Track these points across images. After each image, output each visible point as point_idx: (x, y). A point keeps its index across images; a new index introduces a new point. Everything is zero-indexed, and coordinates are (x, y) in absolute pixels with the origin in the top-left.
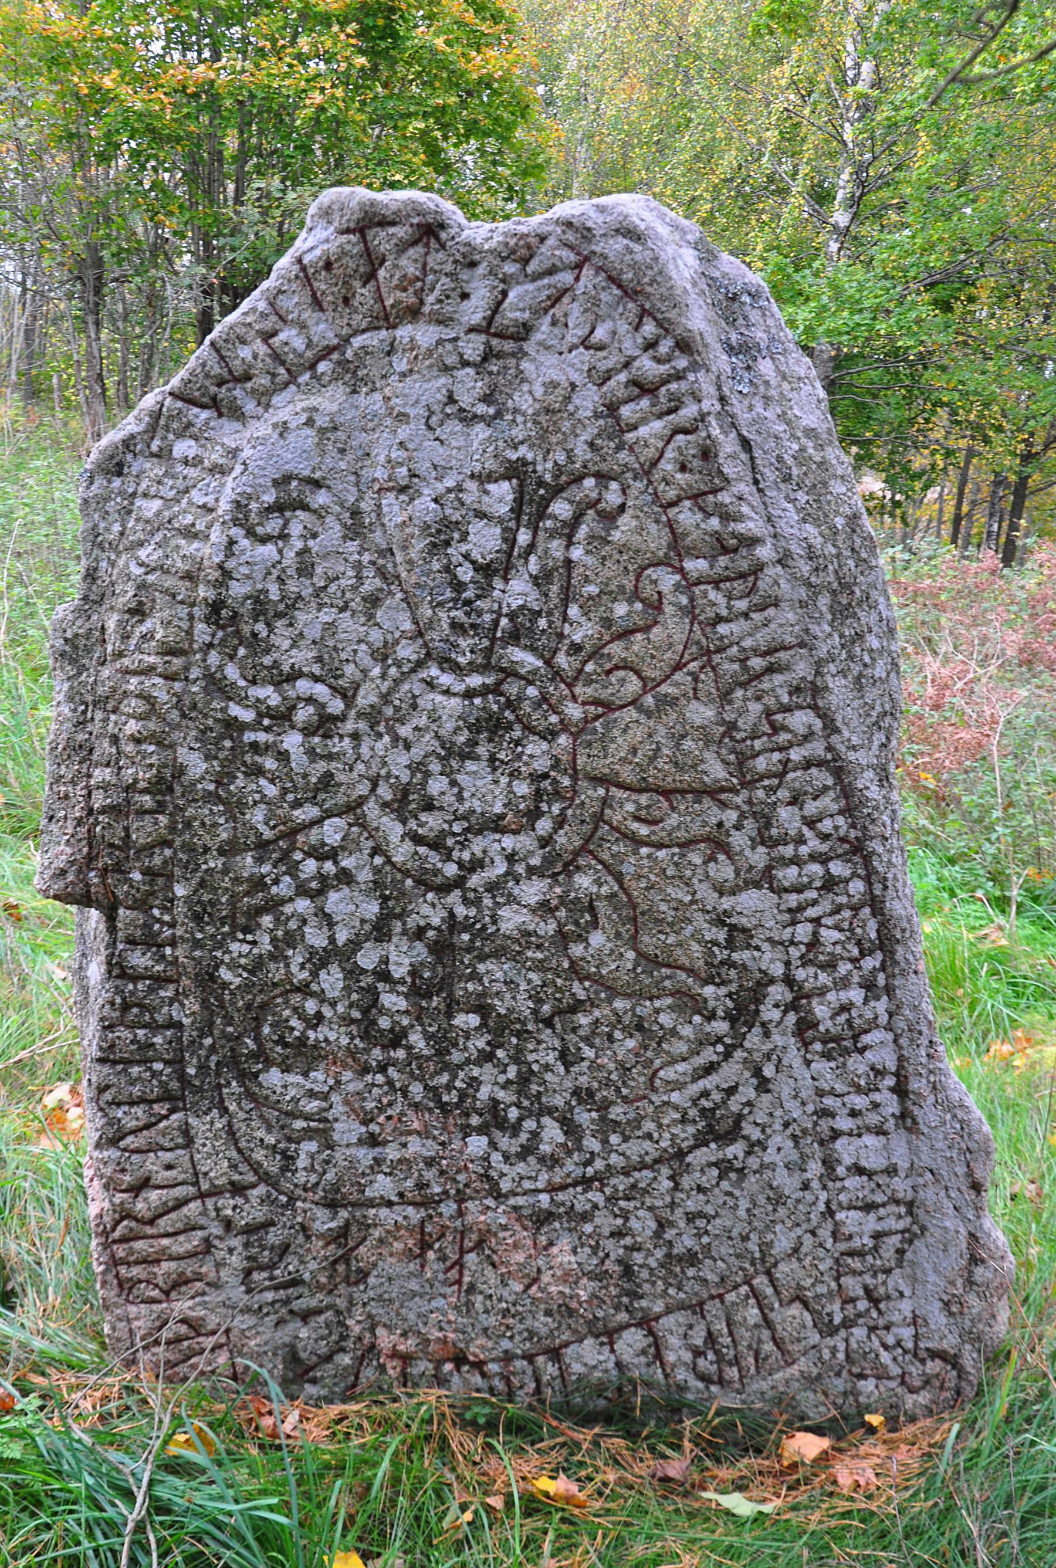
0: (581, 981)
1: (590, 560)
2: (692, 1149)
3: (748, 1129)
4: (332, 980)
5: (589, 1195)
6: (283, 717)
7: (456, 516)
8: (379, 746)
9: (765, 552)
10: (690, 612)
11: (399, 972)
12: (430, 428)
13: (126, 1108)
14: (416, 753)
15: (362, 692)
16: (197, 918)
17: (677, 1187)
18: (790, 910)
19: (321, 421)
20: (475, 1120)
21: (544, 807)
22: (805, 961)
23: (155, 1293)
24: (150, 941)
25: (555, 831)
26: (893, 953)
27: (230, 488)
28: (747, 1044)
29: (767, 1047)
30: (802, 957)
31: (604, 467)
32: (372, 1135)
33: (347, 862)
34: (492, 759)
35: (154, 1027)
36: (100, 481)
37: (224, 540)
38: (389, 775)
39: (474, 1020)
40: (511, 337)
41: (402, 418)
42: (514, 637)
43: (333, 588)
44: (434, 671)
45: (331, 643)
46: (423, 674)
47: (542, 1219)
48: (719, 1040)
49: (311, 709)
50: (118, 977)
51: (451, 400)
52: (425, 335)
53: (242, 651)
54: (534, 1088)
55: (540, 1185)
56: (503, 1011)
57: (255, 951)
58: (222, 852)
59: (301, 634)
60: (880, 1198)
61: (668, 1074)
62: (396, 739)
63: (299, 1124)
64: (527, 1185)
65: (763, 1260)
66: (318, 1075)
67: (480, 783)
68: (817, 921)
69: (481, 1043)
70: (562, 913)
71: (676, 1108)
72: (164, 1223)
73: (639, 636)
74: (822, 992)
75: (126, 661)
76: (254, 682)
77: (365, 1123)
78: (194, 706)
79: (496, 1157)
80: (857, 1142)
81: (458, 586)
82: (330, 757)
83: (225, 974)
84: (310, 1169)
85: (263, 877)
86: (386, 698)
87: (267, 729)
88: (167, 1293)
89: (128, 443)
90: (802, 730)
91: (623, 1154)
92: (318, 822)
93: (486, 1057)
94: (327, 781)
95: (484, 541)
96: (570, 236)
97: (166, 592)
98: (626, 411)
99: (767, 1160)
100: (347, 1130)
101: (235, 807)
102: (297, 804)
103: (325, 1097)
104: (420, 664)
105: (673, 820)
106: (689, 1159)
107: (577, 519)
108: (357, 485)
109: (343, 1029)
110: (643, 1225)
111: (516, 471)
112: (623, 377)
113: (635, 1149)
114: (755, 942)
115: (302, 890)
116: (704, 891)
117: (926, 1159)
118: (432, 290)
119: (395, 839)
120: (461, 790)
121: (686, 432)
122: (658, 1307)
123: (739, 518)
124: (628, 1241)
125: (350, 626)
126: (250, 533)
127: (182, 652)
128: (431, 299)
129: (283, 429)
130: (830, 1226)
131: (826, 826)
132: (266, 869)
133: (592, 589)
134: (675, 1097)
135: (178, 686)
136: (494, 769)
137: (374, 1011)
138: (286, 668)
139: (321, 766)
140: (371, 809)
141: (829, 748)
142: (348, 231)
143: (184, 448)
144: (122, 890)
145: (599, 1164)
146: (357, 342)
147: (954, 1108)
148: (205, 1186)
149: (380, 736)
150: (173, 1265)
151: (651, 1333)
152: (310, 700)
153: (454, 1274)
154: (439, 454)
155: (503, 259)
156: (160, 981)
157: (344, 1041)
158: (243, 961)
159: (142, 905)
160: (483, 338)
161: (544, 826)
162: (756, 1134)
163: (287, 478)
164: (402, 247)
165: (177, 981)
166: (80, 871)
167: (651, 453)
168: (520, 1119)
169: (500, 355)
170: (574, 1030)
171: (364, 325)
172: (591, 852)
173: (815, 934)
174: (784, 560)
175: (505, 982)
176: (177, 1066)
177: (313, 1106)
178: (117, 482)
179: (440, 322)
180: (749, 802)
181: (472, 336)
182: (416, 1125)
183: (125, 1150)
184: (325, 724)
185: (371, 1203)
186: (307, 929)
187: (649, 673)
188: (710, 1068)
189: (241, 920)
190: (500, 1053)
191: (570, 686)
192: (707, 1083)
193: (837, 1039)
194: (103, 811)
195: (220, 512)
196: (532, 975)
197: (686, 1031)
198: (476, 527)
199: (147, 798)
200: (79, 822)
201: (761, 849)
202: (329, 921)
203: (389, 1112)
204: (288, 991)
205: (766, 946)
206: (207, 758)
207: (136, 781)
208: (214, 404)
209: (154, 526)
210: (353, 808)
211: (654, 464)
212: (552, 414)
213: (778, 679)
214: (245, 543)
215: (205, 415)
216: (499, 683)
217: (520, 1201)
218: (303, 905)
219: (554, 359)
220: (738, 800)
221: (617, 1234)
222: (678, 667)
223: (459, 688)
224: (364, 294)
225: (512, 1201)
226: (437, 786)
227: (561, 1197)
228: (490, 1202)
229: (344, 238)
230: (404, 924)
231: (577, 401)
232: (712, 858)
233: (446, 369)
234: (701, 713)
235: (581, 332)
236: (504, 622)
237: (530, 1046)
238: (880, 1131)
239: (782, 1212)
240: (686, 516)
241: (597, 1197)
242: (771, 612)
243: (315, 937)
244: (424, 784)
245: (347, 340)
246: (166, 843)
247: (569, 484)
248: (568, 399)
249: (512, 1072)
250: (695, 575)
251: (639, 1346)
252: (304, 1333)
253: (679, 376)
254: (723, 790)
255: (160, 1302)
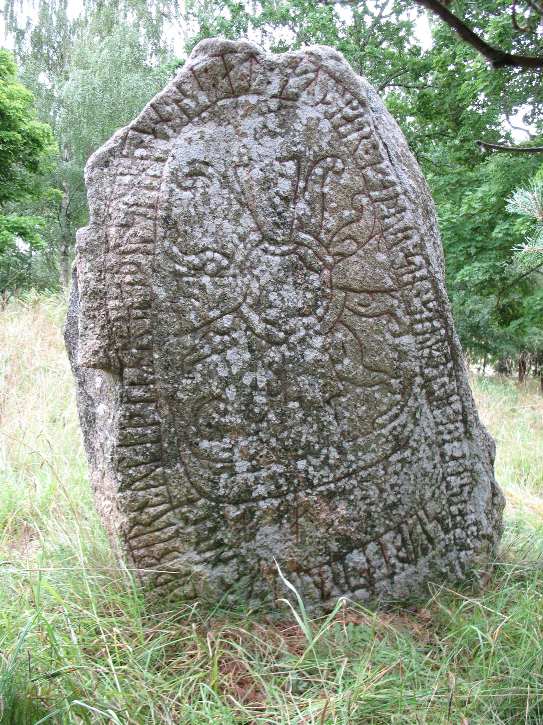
0: (341, 381)
1: (331, 192)
2: (391, 455)
3: (413, 444)
4: (231, 393)
5: (352, 481)
6: (199, 270)
7: (272, 176)
8: (246, 280)
9: (399, 189)
10: (373, 213)
11: (261, 385)
12: (256, 139)
13: (134, 468)
14: (263, 281)
15: (236, 256)
16: (166, 368)
17: (386, 473)
18: (420, 343)
19: (207, 137)
20: (300, 452)
21: (319, 303)
22: (428, 366)
23: (153, 561)
24: (141, 383)
25: (325, 314)
26: (457, 360)
27: (166, 169)
28: (409, 404)
29: (416, 405)
30: (426, 364)
31: (334, 152)
32: (253, 466)
33: (235, 335)
34: (295, 283)
35: (146, 425)
36: (96, 170)
37: (168, 189)
38: (251, 293)
39: (297, 404)
40: (290, 100)
41: (244, 135)
42: (301, 227)
43: (219, 209)
44: (267, 245)
45: (221, 234)
46: (262, 247)
47: (330, 496)
48: (398, 403)
49: (214, 264)
50: (126, 403)
51: (265, 127)
52: (253, 99)
53: (179, 240)
54: (325, 433)
55: (330, 479)
56: (310, 398)
57: (194, 382)
58: (175, 335)
59: (207, 231)
60: (461, 469)
61: (380, 421)
62: (253, 275)
63: (219, 465)
64: (325, 480)
65: (421, 503)
66: (227, 440)
67: (290, 294)
68: (430, 347)
69: (301, 415)
70: (331, 351)
71: (384, 436)
72: (158, 524)
73: (355, 225)
74: (435, 378)
75: (122, 248)
76: (185, 254)
77: (250, 460)
78: (159, 266)
79: (311, 469)
80: (452, 445)
81: (274, 206)
82: (225, 286)
83: (180, 395)
84: (226, 487)
85: (196, 345)
86: (246, 258)
87: (193, 276)
88: (159, 560)
89: (111, 152)
90: (419, 264)
91: (364, 460)
92: (221, 317)
93: (304, 421)
94: (223, 298)
95: (285, 186)
96: (313, 58)
97: (141, 214)
98: (342, 130)
99: (420, 456)
100: (242, 465)
101: (180, 312)
102: (210, 309)
103: (230, 450)
104: (260, 242)
105: (374, 305)
106: (390, 459)
107: (324, 177)
108: (224, 165)
109: (237, 416)
110: (373, 493)
111: (296, 157)
112: (339, 115)
113: (369, 457)
114: (409, 357)
115: (215, 351)
116: (388, 336)
117: (476, 451)
118: (255, 80)
119: (256, 322)
120: (283, 299)
121: (366, 138)
122: (382, 530)
123: (388, 174)
124: (368, 501)
125: (227, 226)
126: (180, 186)
127: (152, 241)
128: (254, 84)
129: (190, 141)
130: (444, 484)
131: (431, 305)
132: (197, 342)
133: (334, 205)
134: (383, 431)
135: (151, 257)
136: (296, 288)
137: (251, 405)
138: (201, 246)
139: (220, 291)
140: (244, 309)
141: (429, 272)
142: (215, 56)
143: (139, 152)
144: (126, 360)
145: (354, 466)
146: (220, 103)
147: (482, 428)
148: (175, 503)
149: (245, 275)
150: (162, 545)
151: (379, 543)
152: (212, 260)
153: (294, 529)
154: (262, 150)
155: (286, 67)
156: (148, 401)
157: (239, 421)
158: (188, 387)
159: (137, 364)
160: (278, 100)
161: (320, 311)
162: (414, 444)
163: (194, 161)
164: (242, 61)
165: (157, 401)
166: (105, 351)
167: (354, 147)
168: (320, 449)
169: (286, 107)
170: (340, 405)
171: (223, 96)
172: (341, 322)
173: (430, 352)
174: (405, 193)
175: (309, 385)
176: (158, 444)
177: (226, 455)
178: (106, 170)
179: (259, 94)
180: (402, 296)
181: (273, 99)
182: (274, 458)
183: (134, 490)
184: (219, 272)
185: (256, 500)
186: (218, 369)
187: (360, 240)
188: (396, 416)
189: (187, 368)
190: (309, 419)
191: (327, 248)
192: (395, 423)
193: (441, 399)
194: (117, 319)
195: (164, 177)
196: (320, 381)
197: (386, 400)
198: (281, 181)
199: (138, 311)
200: (103, 327)
201: (408, 317)
202: (228, 364)
203: (261, 454)
204: (211, 400)
205: (413, 359)
206: (166, 291)
207: (133, 303)
208: (154, 133)
209: (131, 186)
210: (236, 310)
211: (355, 150)
212: (311, 130)
213: (409, 242)
214: (177, 190)
215: (150, 137)
216: (295, 249)
217: (322, 488)
218: (215, 357)
219: (310, 109)
220: (398, 294)
221: (364, 498)
222: (371, 237)
223: (278, 252)
224: (223, 83)
225: (319, 489)
226: (273, 297)
227: (339, 484)
228: (309, 491)
229: (213, 59)
230: (263, 362)
231: (321, 125)
232: (389, 321)
233: (262, 114)
234: (382, 257)
235: (321, 97)
236: (296, 221)
237: (322, 414)
238: (459, 440)
239: (427, 479)
240: (369, 172)
241: (355, 482)
242: (403, 214)
243: (223, 372)
244: (267, 296)
245: (215, 103)
246: (148, 332)
247: (320, 160)
248: (317, 125)
249: (315, 427)
250: (375, 198)
251: (375, 550)
252: (226, 569)
253: (361, 115)
254: (392, 290)
255: (156, 565)
